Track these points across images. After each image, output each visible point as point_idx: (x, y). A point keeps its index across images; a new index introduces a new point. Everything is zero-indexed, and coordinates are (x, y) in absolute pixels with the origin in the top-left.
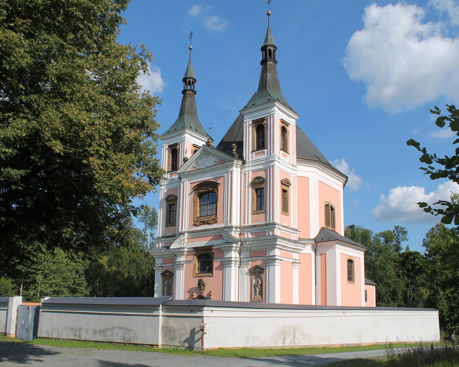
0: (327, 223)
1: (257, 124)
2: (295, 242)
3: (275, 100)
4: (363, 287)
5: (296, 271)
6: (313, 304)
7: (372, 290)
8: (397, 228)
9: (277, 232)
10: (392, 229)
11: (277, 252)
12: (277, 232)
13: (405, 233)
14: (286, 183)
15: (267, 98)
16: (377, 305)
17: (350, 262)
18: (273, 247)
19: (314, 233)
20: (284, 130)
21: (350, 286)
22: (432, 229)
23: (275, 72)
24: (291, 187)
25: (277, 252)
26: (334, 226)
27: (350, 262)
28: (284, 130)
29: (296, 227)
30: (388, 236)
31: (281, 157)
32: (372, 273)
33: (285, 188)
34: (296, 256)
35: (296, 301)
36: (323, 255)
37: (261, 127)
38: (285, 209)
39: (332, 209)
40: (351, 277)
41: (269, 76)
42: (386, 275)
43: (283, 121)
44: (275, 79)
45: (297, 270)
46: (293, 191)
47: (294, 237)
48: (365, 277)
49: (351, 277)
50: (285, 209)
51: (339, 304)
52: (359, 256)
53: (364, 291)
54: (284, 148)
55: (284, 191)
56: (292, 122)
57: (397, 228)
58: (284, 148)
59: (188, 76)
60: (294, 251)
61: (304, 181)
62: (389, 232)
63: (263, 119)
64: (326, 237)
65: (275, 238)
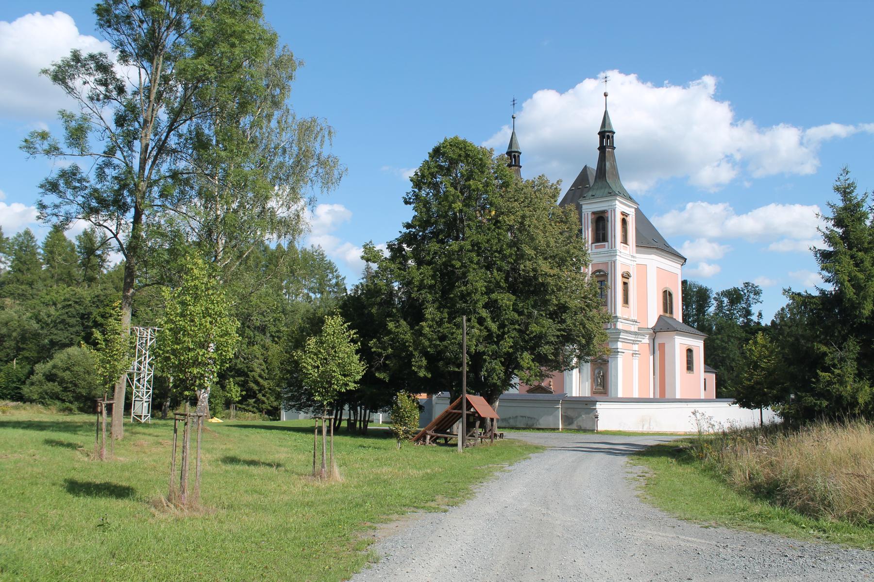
0: (665, 311)
1: (597, 216)
2: (635, 334)
3: (616, 195)
4: (702, 375)
5: (636, 362)
6: (652, 396)
7: (712, 378)
8: (747, 284)
9: (620, 326)
10: (740, 286)
11: (620, 345)
12: (620, 326)
13: (757, 293)
14: (626, 276)
15: (607, 191)
16: (717, 397)
17: (690, 351)
18: (617, 340)
19: (652, 322)
20: (624, 222)
21: (690, 375)
22: (783, 309)
23: (614, 160)
24: (631, 279)
25: (620, 345)
26: (671, 313)
27: (690, 351)
28: (624, 222)
29: (636, 319)
30: (735, 296)
31: (622, 251)
32: (713, 360)
33: (626, 280)
34: (636, 347)
35: (636, 395)
36: (662, 346)
37: (601, 221)
38: (626, 301)
39: (670, 294)
40: (690, 367)
41: (608, 164)
42: (728, 356)
43: (623, 214)
44: (614, 167)
45: (637, 361)
46: (632, 282)
47: (634, 328)
48: (706, 362)
49: (690, 367)
50: (626, 301)
51: (678, 396)
52: (698, 345)
53: (702, 379)
54: (625, 241)
55: (625, 284)
56: (631, 212)
57: (747, 284)
58: (625, 241)
59: (513, 150)
60: (634, 342)
61: (642, 268)
62: (736, 291)
63: (604, 212)
64: (664, 326)
65: (619, 332)
